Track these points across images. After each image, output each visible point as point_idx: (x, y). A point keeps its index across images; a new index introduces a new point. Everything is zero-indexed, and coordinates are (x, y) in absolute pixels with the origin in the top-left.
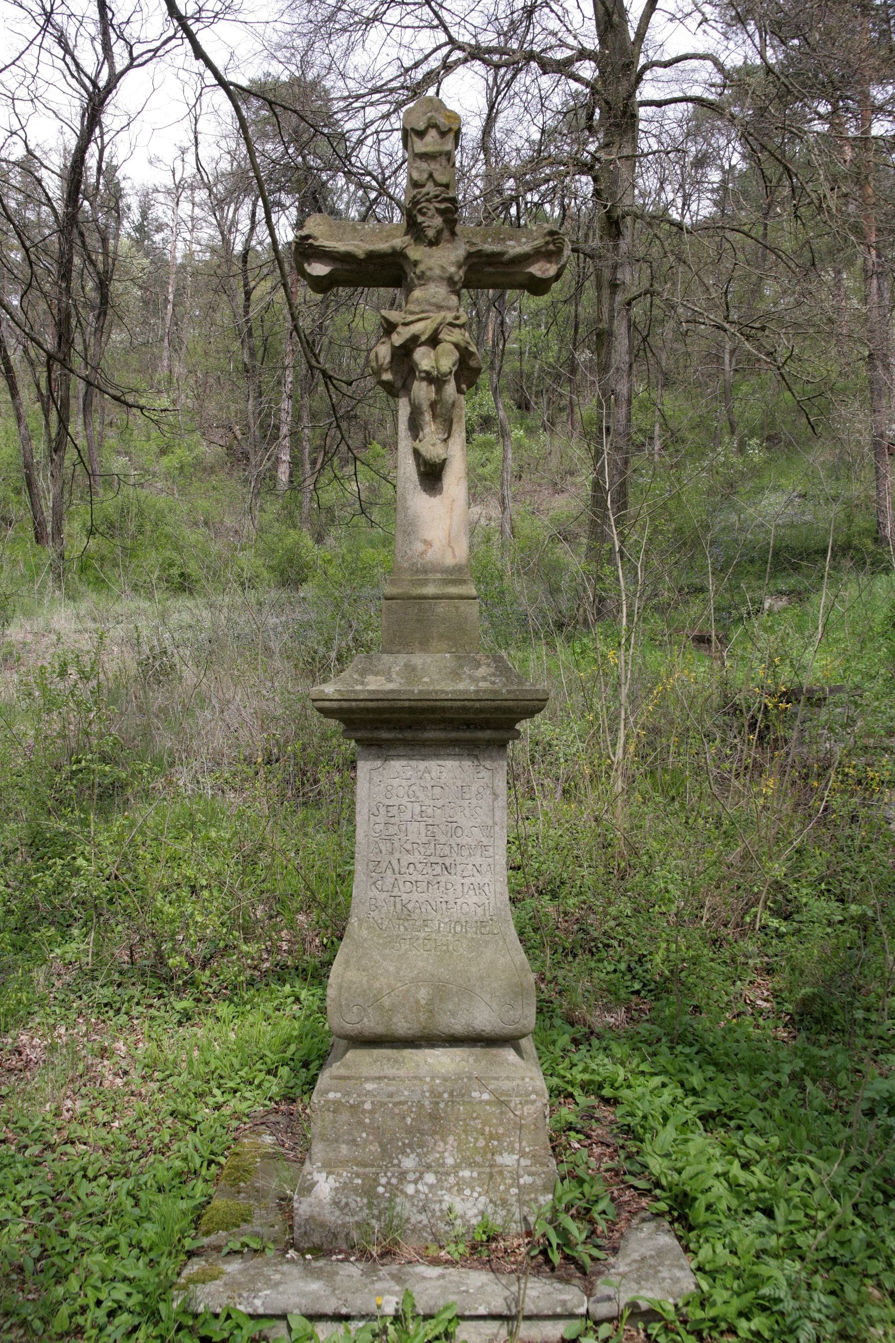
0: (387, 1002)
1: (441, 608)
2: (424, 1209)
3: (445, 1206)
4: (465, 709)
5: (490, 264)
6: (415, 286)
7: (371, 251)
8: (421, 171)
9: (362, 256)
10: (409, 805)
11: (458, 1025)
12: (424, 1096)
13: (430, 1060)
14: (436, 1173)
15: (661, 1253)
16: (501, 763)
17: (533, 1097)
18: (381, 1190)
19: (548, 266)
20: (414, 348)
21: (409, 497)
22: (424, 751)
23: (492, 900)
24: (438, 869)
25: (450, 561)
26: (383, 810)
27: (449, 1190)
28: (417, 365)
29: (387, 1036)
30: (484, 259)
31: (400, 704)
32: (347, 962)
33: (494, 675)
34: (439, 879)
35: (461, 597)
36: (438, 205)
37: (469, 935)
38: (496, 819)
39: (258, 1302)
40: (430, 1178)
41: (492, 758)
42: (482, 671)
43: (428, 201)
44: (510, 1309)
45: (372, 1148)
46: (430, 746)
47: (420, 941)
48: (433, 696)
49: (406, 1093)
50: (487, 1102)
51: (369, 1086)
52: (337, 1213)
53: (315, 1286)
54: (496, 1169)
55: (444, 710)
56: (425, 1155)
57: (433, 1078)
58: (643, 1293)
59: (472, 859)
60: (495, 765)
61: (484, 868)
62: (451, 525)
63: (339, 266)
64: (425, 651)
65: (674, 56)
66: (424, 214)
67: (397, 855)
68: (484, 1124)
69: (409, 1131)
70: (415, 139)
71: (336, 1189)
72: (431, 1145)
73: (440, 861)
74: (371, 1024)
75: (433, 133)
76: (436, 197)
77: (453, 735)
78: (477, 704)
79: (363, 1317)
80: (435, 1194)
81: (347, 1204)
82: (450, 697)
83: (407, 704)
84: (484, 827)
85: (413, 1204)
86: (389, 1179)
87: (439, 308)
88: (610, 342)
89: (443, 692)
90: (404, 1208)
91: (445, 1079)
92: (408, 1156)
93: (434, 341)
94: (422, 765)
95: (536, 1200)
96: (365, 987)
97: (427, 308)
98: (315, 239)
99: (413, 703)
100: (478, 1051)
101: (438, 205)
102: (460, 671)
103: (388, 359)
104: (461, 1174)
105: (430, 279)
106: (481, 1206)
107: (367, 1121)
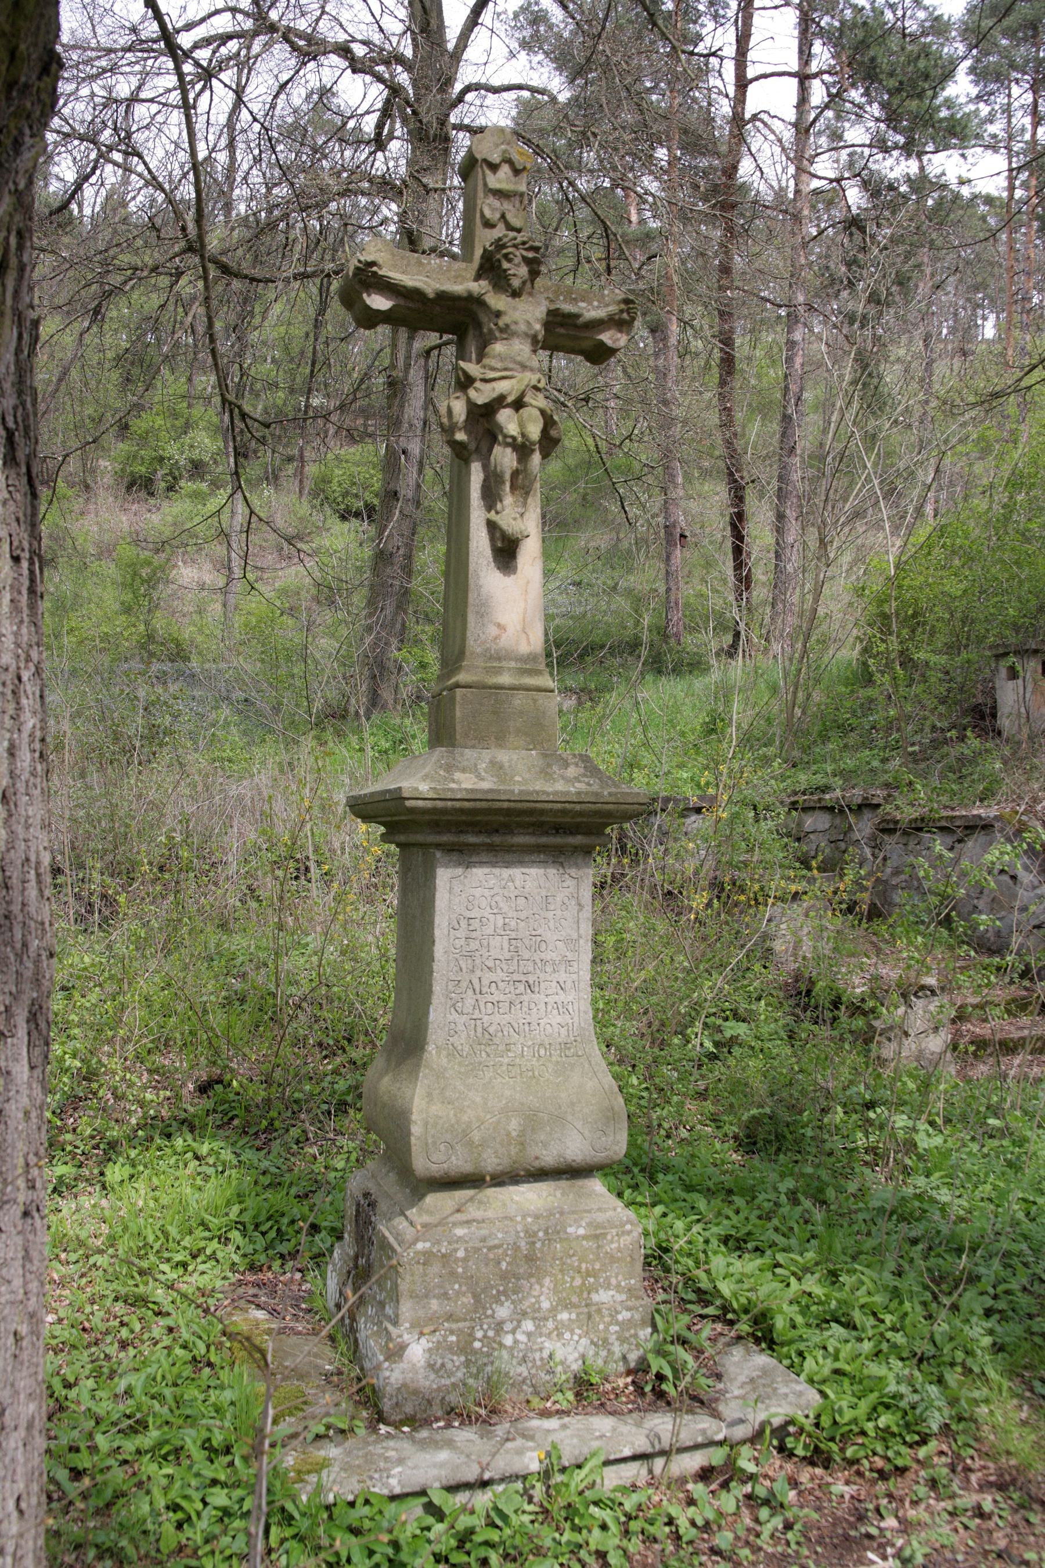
0: (476, 1136)
1: (519, 700)
2: (524, 1360)
3: (545, 1354)
4: (564, 812)
5: (562, 325)
6: (496, 339)
7: (443, 292)
8: (493, 210)
9: (431, 296)
10: (492, 917)
11: (549, 1158)
12: (518, 1237)
13: (516, 1198)
14: (534, 1319)
15: (765, 1372)
16: (587, 870)
17: (628, 1227)
18: (477, 1345)
19: (619, 335)
20: (498, 409)
21: (482, 574)
22: (508, 857)
23: (576, 1019)
24: (521, 988)
25: (524, 649)
26: (464, 923)
27: (549, 1336)
28: (501, 429)
29: (474, 1174)
30: (559, 319)
31: (498, 805)
32: (429, 1095)
33: (585, 775)
34: (522, 998)
35: (539, 689)
36: (525, 253)
37: (554, 1059)
38: (582, 932)
39: (393, 1482)
40: (528, 1325)
41: (578, 867)
42: (572, 771)
43: (515, 246)
44: (653, 1446)
45: (465, 1300)
46: (514, 852)
47: (504, 1068)
48: (534, 798)
49: (500, 1235)
50: (585, 1237)
51: (460, 1232)
52: (433, 1376)
53: (444, 1455)
54: (594, 1308)
55: (542, 812)
56: (520, 1301)
57: (524, 1217)
58: (773, 1410)
59: (556, 975)
60: (581, 873)
61: (569, 984)
62: (525, 609)
63: (402, 302)
64: (501, 746)
65: (506, 83)
66: (510, 261)
67: (478, 973)
68: (580, 1261)
69: (504, 1277)
70: (488, 172)
71: (430, 1350)
72: (527, 1290)
73: (523, 978)
74: (459, 1163)
75: (505, 169)
76: (524, 243)
77: (544, 840)
78: (578, 807)
79: (502, 1480)
80: (535, 1343)
81: (443, 1365)
82: (551, 798)
83: (506, 805)
84: (567, 941)
85: (513, 1356)
86: (486, 1331)
87: (524, 367)
88: (404, 393)
89: (544, 792)
90: (505, 1361)
91: (537, 1217)
92: (502, 1305)
93: (518, 405)
94: (506, 873)
95: (636, 1336)
96: (453, 1121)
97: (511, 366)
98: (380, 267)
99: (512, 805)
100: (564, 1183)
101: (525, 253)
102: (549, 770)
103: (463, 418)
104: (559, 1317)
105: (514, 334)
106: (581, 1349)
107: (460, 1270)
